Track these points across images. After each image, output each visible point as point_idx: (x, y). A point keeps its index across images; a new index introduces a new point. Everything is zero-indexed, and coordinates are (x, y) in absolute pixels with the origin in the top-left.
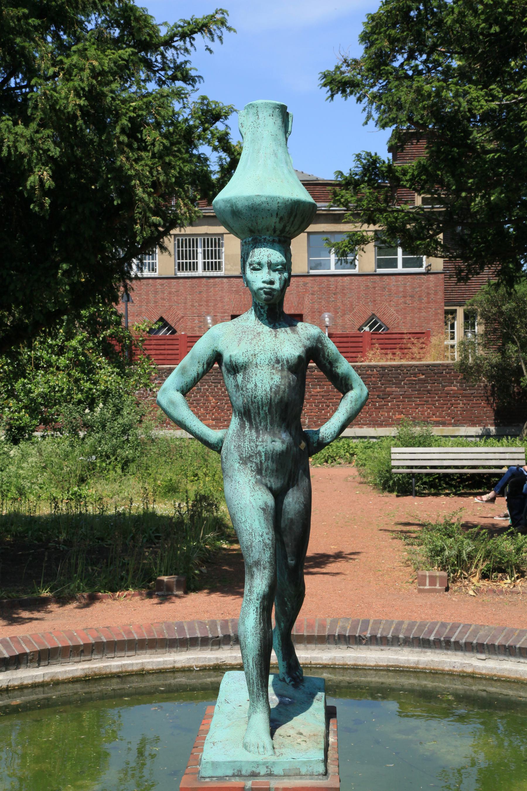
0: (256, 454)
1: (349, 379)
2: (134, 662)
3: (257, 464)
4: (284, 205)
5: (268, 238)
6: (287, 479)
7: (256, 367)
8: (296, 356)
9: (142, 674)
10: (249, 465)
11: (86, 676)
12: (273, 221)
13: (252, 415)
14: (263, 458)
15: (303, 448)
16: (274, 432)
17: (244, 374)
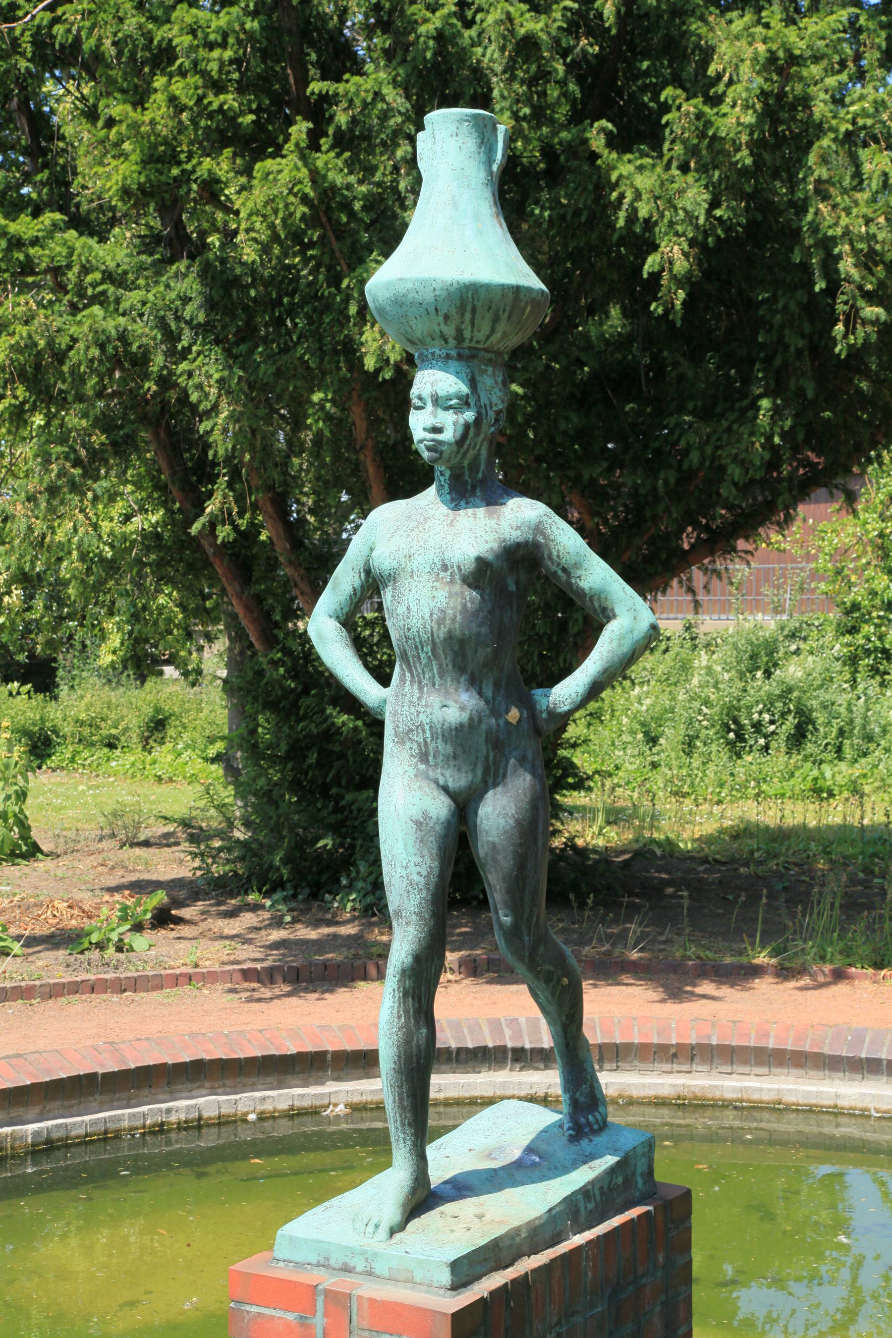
2: (765, 1086)
3: (419, 745)
4: (445, 294)
5: (438, 352)
6: (479, 771)
7: (412, 577)
9: (778, 1109)
10: (408, 745)
11: (679, 1098)
12: (436, 324)
14: (428, 734)
15: (514, 721)
17: (394, 589)
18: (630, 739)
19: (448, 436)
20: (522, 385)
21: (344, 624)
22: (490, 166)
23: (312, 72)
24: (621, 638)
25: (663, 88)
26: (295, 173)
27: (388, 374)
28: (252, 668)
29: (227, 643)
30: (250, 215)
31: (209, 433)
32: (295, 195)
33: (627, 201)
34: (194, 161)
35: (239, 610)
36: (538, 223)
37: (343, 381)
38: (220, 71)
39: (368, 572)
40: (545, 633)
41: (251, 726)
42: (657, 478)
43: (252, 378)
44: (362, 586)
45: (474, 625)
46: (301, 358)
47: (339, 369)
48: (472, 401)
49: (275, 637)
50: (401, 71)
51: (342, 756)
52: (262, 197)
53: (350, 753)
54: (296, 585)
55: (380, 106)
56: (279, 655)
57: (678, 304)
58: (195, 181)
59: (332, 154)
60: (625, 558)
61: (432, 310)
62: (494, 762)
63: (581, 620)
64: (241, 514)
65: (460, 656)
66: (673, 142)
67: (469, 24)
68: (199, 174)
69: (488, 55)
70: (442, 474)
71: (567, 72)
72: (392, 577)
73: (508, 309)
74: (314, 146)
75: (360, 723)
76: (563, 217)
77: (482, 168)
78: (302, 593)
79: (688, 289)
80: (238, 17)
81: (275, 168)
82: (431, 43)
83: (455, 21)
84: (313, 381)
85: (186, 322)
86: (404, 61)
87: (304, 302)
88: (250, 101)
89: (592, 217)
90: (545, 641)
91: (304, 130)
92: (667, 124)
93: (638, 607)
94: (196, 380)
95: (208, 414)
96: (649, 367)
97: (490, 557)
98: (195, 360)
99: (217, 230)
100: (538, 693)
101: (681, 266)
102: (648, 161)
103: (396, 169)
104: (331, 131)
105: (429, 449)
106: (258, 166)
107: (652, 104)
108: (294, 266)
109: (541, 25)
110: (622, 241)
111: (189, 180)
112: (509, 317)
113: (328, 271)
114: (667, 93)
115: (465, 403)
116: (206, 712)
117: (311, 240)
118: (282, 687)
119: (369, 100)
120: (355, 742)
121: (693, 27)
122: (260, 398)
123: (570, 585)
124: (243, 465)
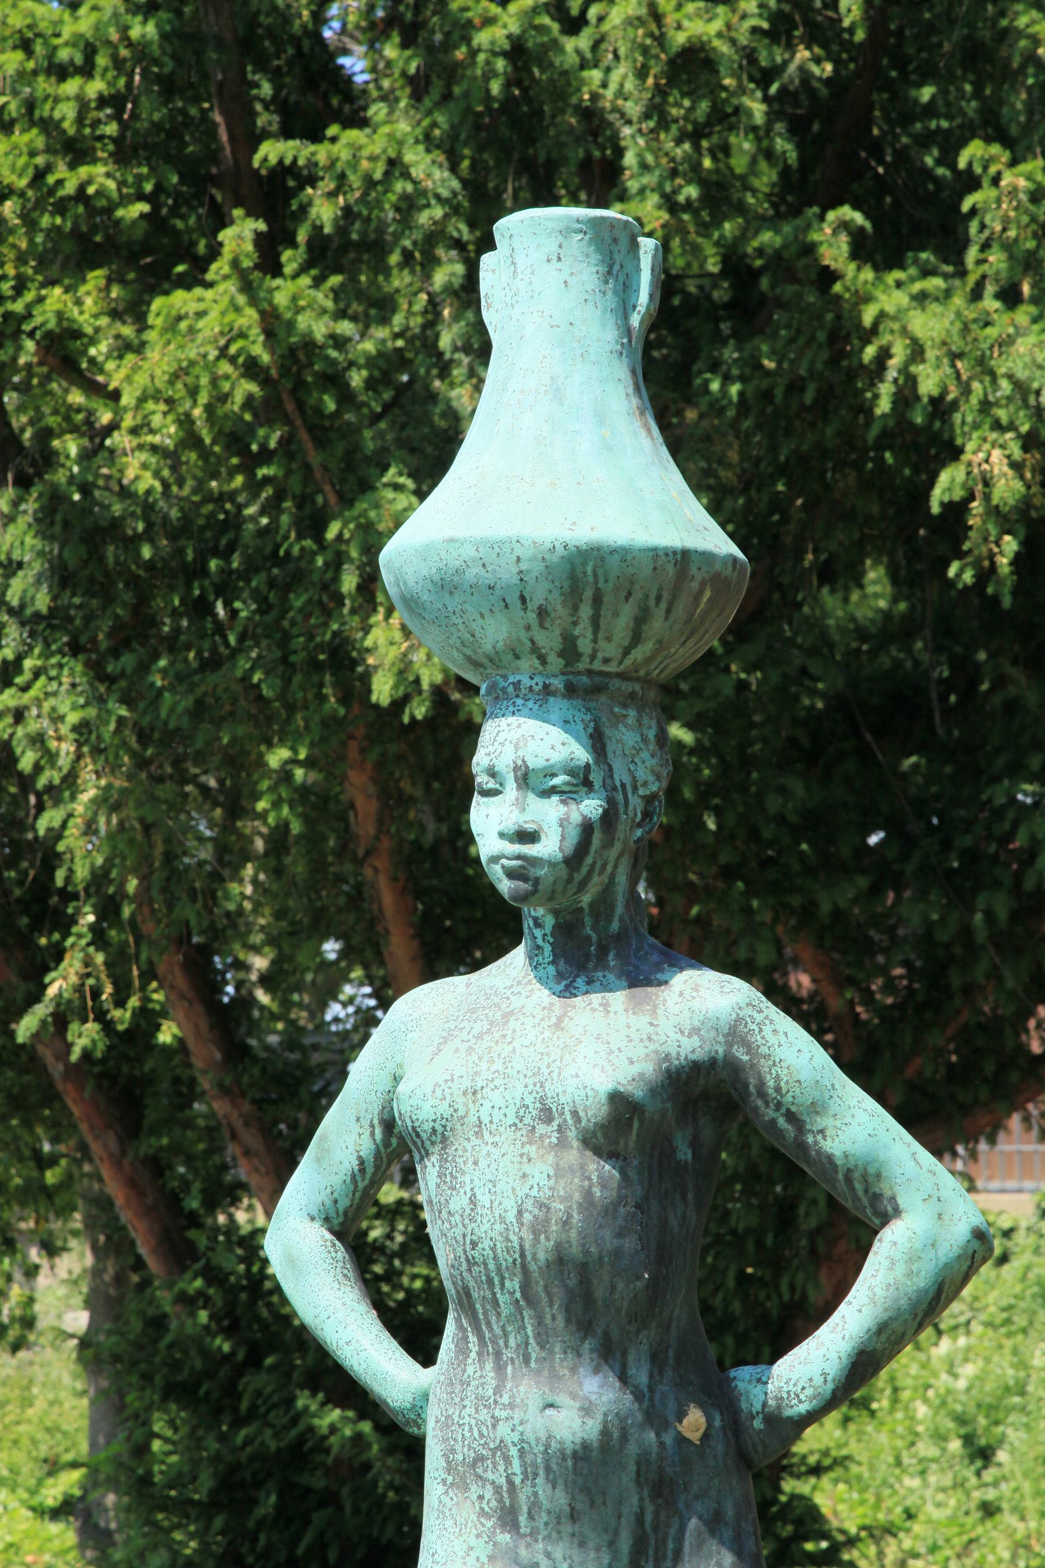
0: (494, 1451)
1: (878, 1176)
3: (497, 1490)
4: (538, 568)
5: (526, 682)
7: (479, 1134)
8: (603, 1098)
10: (475, 1490)
13: (478, 1306)
14: (516, 1466)
15: (695, 1437)
16: (552, 1369)
17: (443, 1160)
18: (933, 1452)
19: (550, 847)
20: (689, 726)
21: (339, 1234)
22: (626, 317)
23: (264, 119)
24: (913, 1257)
25: (963, 143)
26: (231, 316)
27: (419, 710)
28: (142, 1313)
29: (89, 1260)
30: (142, 400)
31: (57, 834)
32: (233, 360)
33: (894, 363)
34: (29, 296)
35: (114, 1188)
36: (717, 407)
37: (331, 723)
38: (80, 120)
39: (389, 1125)
40: (748, 1230)
41: (138, 1435)
42: (972, 911)
43: (146, 721)
44: (377, 1155)
45: (607, 1234)
46: (246, 678)
47: (322, 698)
48: (596, 778)
49: (191, 1245)
50: (441, 119)
51: (329, 1498)
52: (167, 367)
53: (345, 1491)
54: (234, 1136)
55: (400, 186)
56: (198, 1283)
57: (1004, 562)
58: (31, 335)
59: (305, 281)
60: (910, 1072)
61: (514, 600)
62: (656, 1529)
63: (822, 1203)
64: (120, 1002)
65: (584, 1300)
66: (985, 246)
67: (574, 25)
68: (38, 320)
69: (613, 86)
70: (538, 924)
71: (772, 116)
72: (441, 1136)
73: (666, 595)
74: (270, 263)
75: (366, 1427)
76: (767, 396)
77: (611, 322)
78: (247, 1153)
79: (1022, 533)
80: (116, 15)
81: (192, 307)
82: (500, 64)
83: (546, 20)
84: (270, 726)
85: (11, 611)
86: (447, 97)
87: (251, 568)
88: (140, 179)
89: (826, 395)
90: (751, 1247)
91: (249, 235)
92: (973, 211)
93: (944, 1194)
94: (33, 726)
95: (54, 794)
96: (947, 686)
97: (638, 1093)
98: (25, 689)
99: (74, 429)
100: (743, 1374)
101: (1008, 488)
102: (935, 283)
103: (433, 306)
104: (302, 236)
105: (511, 874)
106: (158, 303)
107: (941, 171)
108: (232, 496)
109: (717, 25)
110: (886, 439)
111: (19, 332)
112: (668, 611)
113: (300, 506)
114: (972, 153)
115: (582, 781)
116: (40, 1405)
117: (263, 447)
118: (205, 1353)
119: (378, 175)
120: (355, 1467)
121: (1022, 21)
122: (158, 757)
123: (802, 1146)
124: (125, 895)
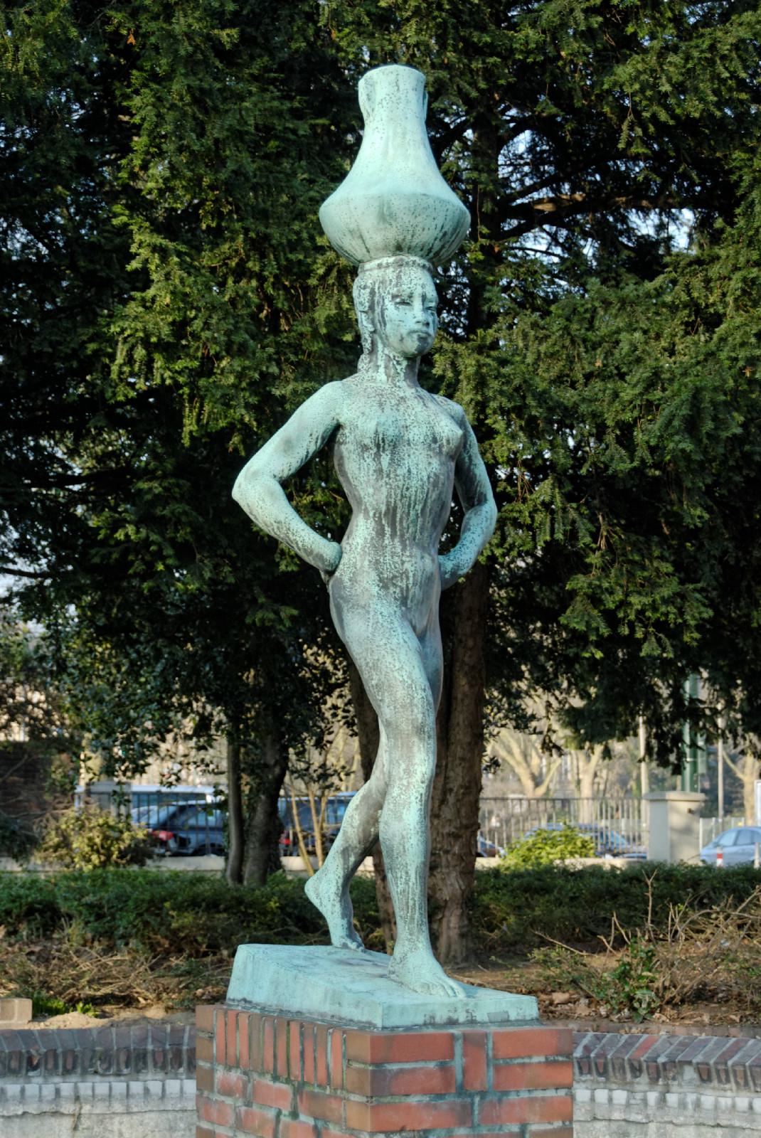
10: (392, 589)
13: (398, 516)
14: (411, 580)
123: (469, 469)
